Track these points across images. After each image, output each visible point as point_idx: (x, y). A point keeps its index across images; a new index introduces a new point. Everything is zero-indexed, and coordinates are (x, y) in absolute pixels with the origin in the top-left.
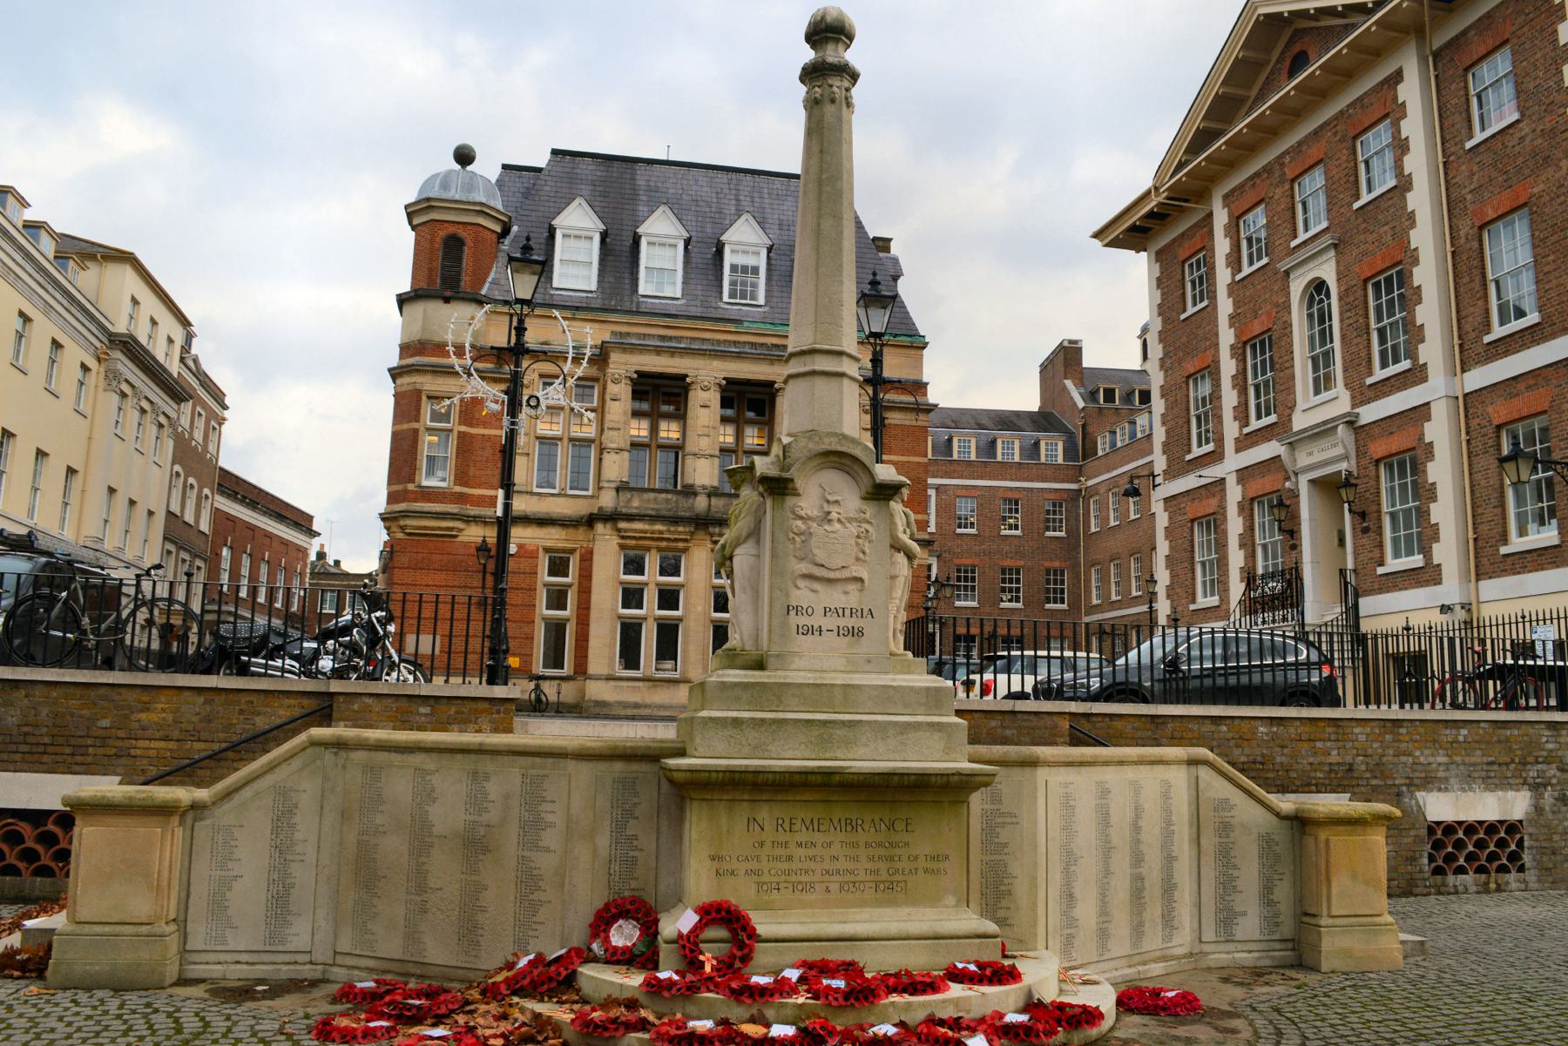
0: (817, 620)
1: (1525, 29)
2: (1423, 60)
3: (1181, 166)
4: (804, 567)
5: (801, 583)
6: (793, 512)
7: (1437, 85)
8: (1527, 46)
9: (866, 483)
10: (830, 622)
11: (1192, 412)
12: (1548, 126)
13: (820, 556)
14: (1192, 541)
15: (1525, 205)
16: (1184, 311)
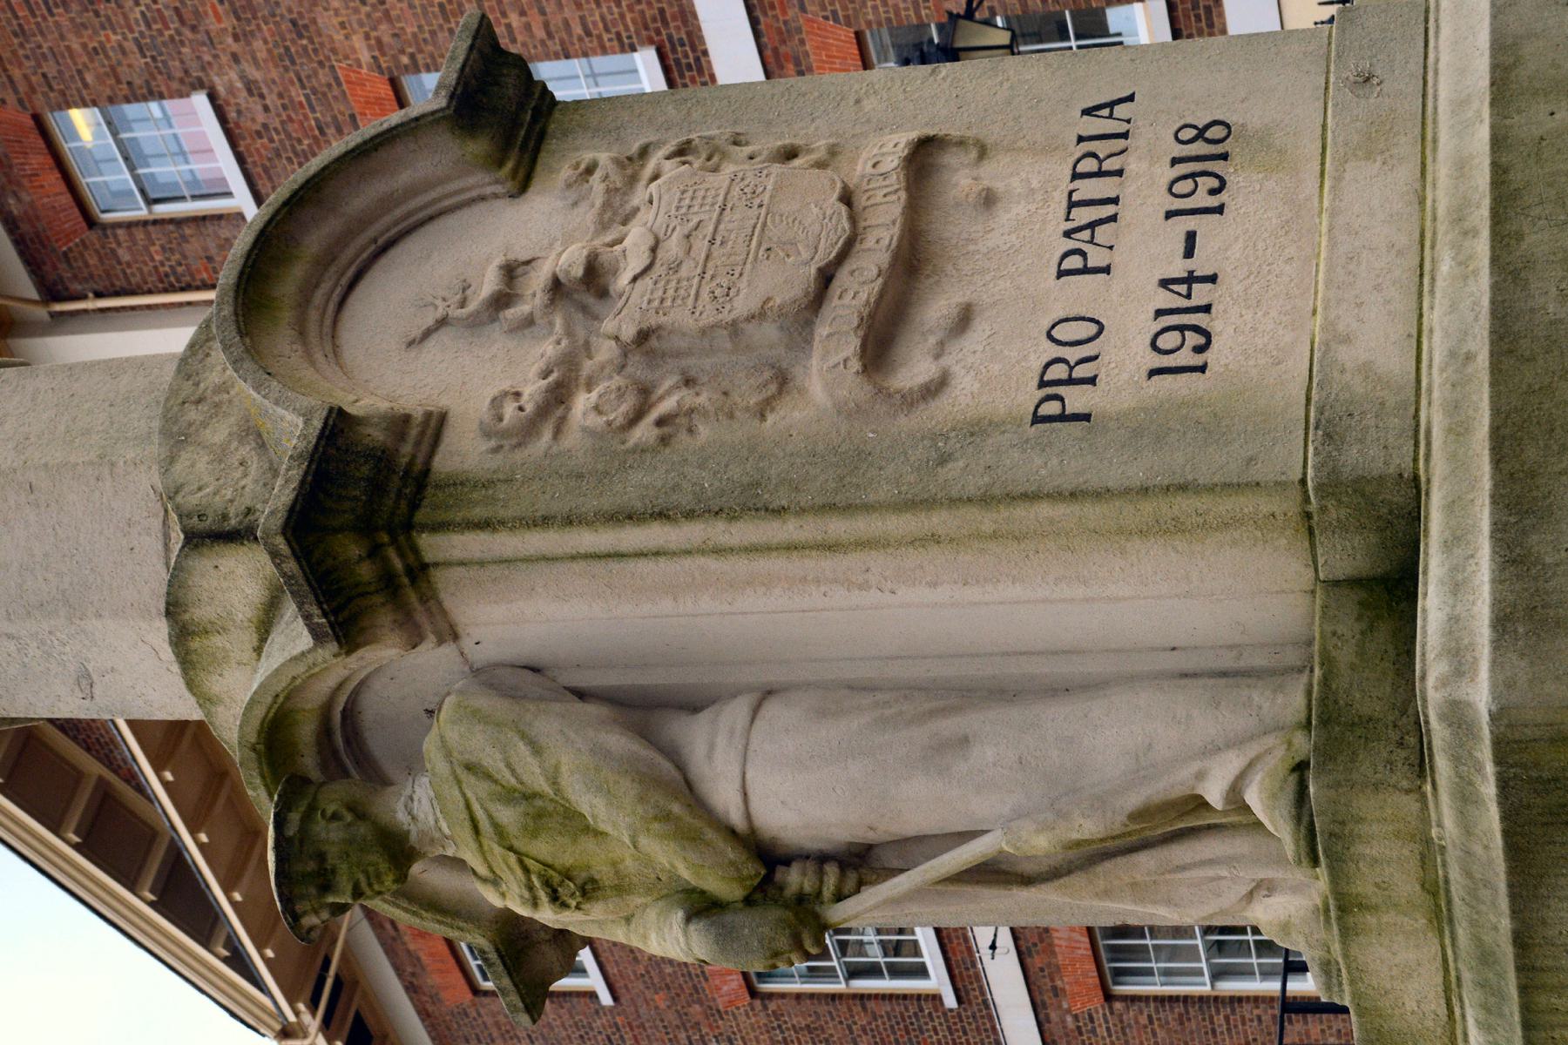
0: (1130, 306)
1: (17, 74)
2: (60, 323)
3: (238, 961)
4: (828, 368)
5: (914, 369)
6: (529, 429)
7: (118, 294)
8: (50, 68)
9: (440, 161)
10: (1145, 248)
11: (840, 987)
12: (229, 23)
13: (786, 280)
14: (1161, 1000)
15: (395, 84)
16: (592, 995)
